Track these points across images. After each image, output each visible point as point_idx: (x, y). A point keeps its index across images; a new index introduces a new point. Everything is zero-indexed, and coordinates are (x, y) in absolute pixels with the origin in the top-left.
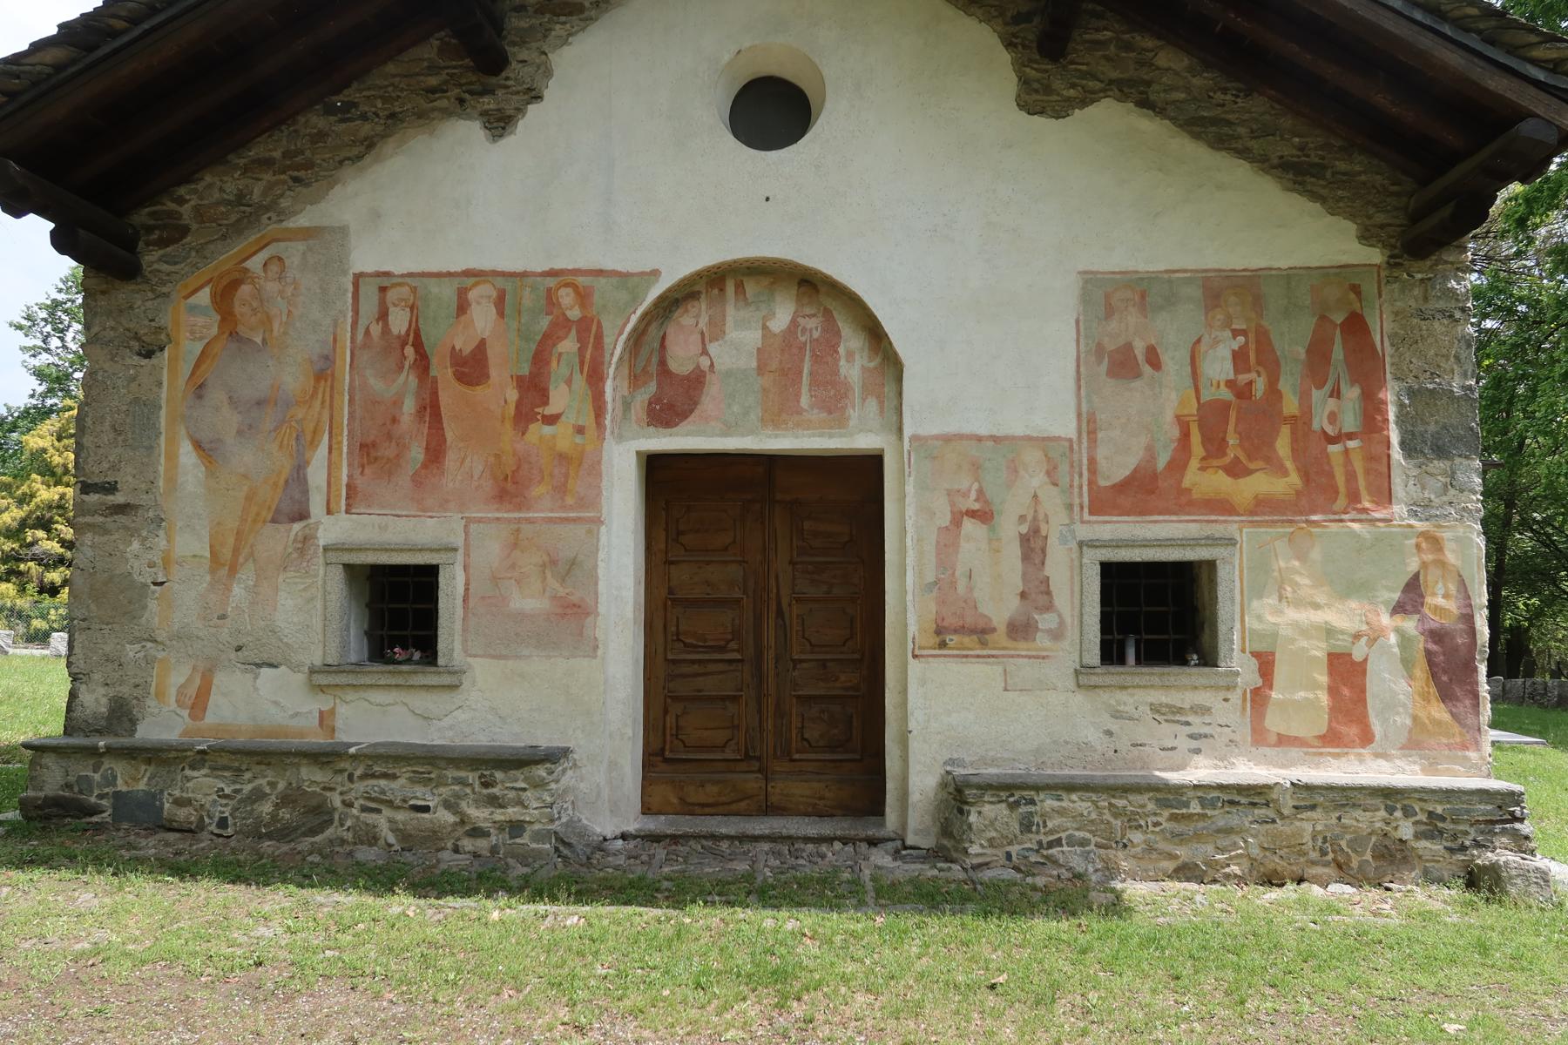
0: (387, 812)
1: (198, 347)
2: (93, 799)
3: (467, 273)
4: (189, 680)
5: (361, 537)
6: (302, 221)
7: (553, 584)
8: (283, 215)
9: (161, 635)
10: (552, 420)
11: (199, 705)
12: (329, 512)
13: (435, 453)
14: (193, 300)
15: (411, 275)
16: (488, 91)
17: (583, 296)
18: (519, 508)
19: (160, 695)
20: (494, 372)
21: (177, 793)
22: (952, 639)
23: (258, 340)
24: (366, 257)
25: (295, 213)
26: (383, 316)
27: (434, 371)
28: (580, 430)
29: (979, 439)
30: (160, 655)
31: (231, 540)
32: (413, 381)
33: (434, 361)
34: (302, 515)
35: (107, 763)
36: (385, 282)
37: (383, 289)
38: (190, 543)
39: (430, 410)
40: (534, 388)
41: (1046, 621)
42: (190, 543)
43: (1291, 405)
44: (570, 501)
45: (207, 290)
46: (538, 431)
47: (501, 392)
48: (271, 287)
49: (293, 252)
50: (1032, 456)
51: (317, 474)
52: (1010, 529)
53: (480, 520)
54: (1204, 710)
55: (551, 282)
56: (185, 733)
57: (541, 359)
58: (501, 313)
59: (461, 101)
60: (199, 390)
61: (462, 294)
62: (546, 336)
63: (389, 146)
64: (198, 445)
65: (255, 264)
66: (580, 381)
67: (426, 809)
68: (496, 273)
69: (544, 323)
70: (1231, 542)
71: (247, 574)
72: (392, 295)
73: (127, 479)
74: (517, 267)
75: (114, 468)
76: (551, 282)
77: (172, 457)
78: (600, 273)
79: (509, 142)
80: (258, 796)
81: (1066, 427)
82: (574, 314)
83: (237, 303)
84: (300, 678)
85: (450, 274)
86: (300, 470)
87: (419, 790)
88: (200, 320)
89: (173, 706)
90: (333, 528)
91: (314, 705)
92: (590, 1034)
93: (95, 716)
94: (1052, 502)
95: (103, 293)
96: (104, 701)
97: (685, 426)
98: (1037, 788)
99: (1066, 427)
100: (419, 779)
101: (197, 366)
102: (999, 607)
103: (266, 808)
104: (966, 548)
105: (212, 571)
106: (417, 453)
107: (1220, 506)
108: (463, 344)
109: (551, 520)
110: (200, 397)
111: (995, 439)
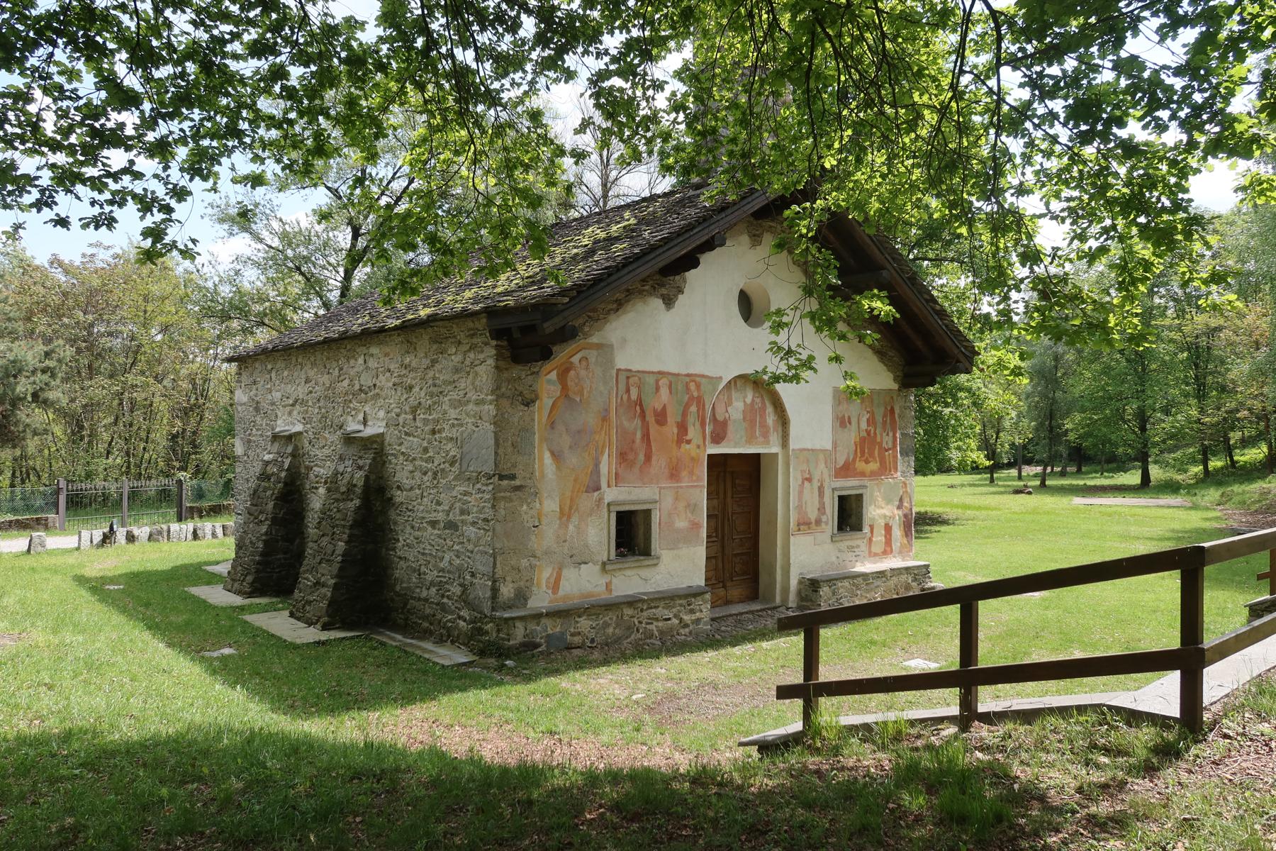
0: (655, 623)
1: (550, 402)
2: (538, 640)
3: (660, 373)
4: (552, 574)
5: (621, 498)
6: (594, 339)
7: (689, 515)
8: (586, 335)
9: (538, 553)
10: (689, 442)
11: (556, 587)
12: (609, 486)
13: (648, 458)
14: (548, 377)
15: (638, 372)
16: (663, 285)
17: (698, 386)
18: (678, 481)
19: (539, 585)
20: (669, 419)
21: (572, 630)
22: (802, 527)
23: (578, 400)
24: (623, 361)
25: (591, 335)
26: (628, 391)
27: (647, 419)
28: (698, 447)
29: (808, 450)
30: (538, 563)
31: (568, 502)
32: (640, 423)
33: (647, 413)
34: (598, 488)
35: (544, 621)
36: (629, 374)
37: (628, 378)
38: (550, 505)
39: (646, 437)
40: (683, 428)
41: (824, 518)
42: (550, 505)
43: (879, 440)
44: (694, 478)
45: (555, 372)
46: (685, 447)
47: (671, 429)
48: (583, 373)
49: (592, 355)
50: (821, 456)
51: (604, 469)
52: (816, 484)
53: (664, 488)
54: (858, 546)
55: (687, 379)
56: (551, 602)
57: (685, 414)
58: (671, 392)
59: (655, 288)
60: (552, 425)
61: (657, 382)
62: (687, 404)
63: (629, 307)
64: (553, 454)
65: (575, 359)
66: (698, 425)
67: (669, 619)
68: (669, 374)
69: (686, 398)
70: (865, 487)
71: (575, 519)
72: (631, 381)
73: (519, 472)
74: (676, 371)
75: (514, 466)
76: (687, 379)
77: (541, 459)
78: (703, 376)
79: (673, 311)
80: (606, 625)
81: (829, 446)
82: (695, 394)
83: (569, 379)
84: (598, 568)
85: (653, 373)
86: (597, 465)
87: (666, 612)
88: (552, 388)
89: (545, 589)
90: (611, 494)
91: (603, 581)
92: (866, 661)
93: (509, 599)
94: (826, 472)
95: (507, 369)
96: (512, 590)
97: (723, 443)
98: (836, 580)
99: (828, 446)
100: (667, 607)
101: (551, 412)
102: (813, 515)
103: (610, 630)
104: (806, 491)
105: (560, 518)
106: (641, 457)
107: (863, 474)
108: (659, 407)
109: (688, 487)
110: (553, 428)
111: (812, 450)
